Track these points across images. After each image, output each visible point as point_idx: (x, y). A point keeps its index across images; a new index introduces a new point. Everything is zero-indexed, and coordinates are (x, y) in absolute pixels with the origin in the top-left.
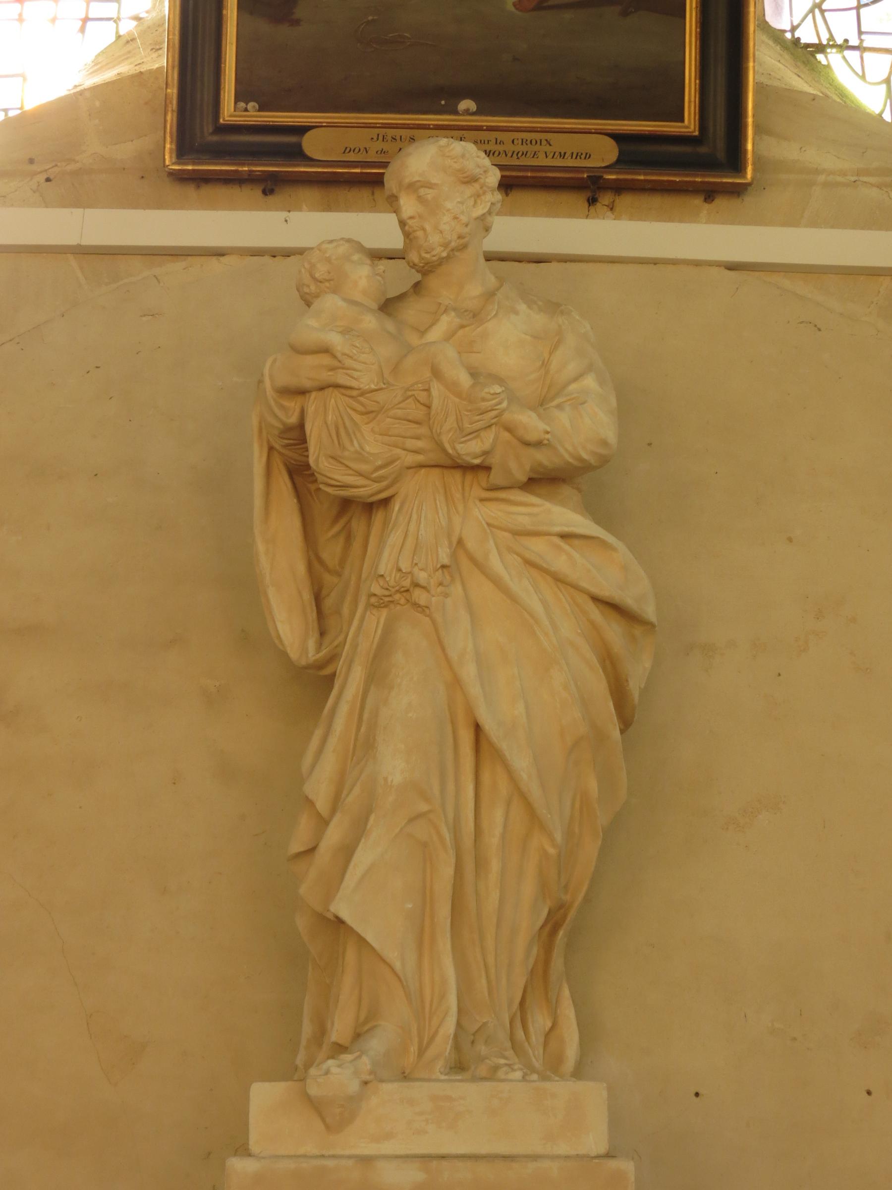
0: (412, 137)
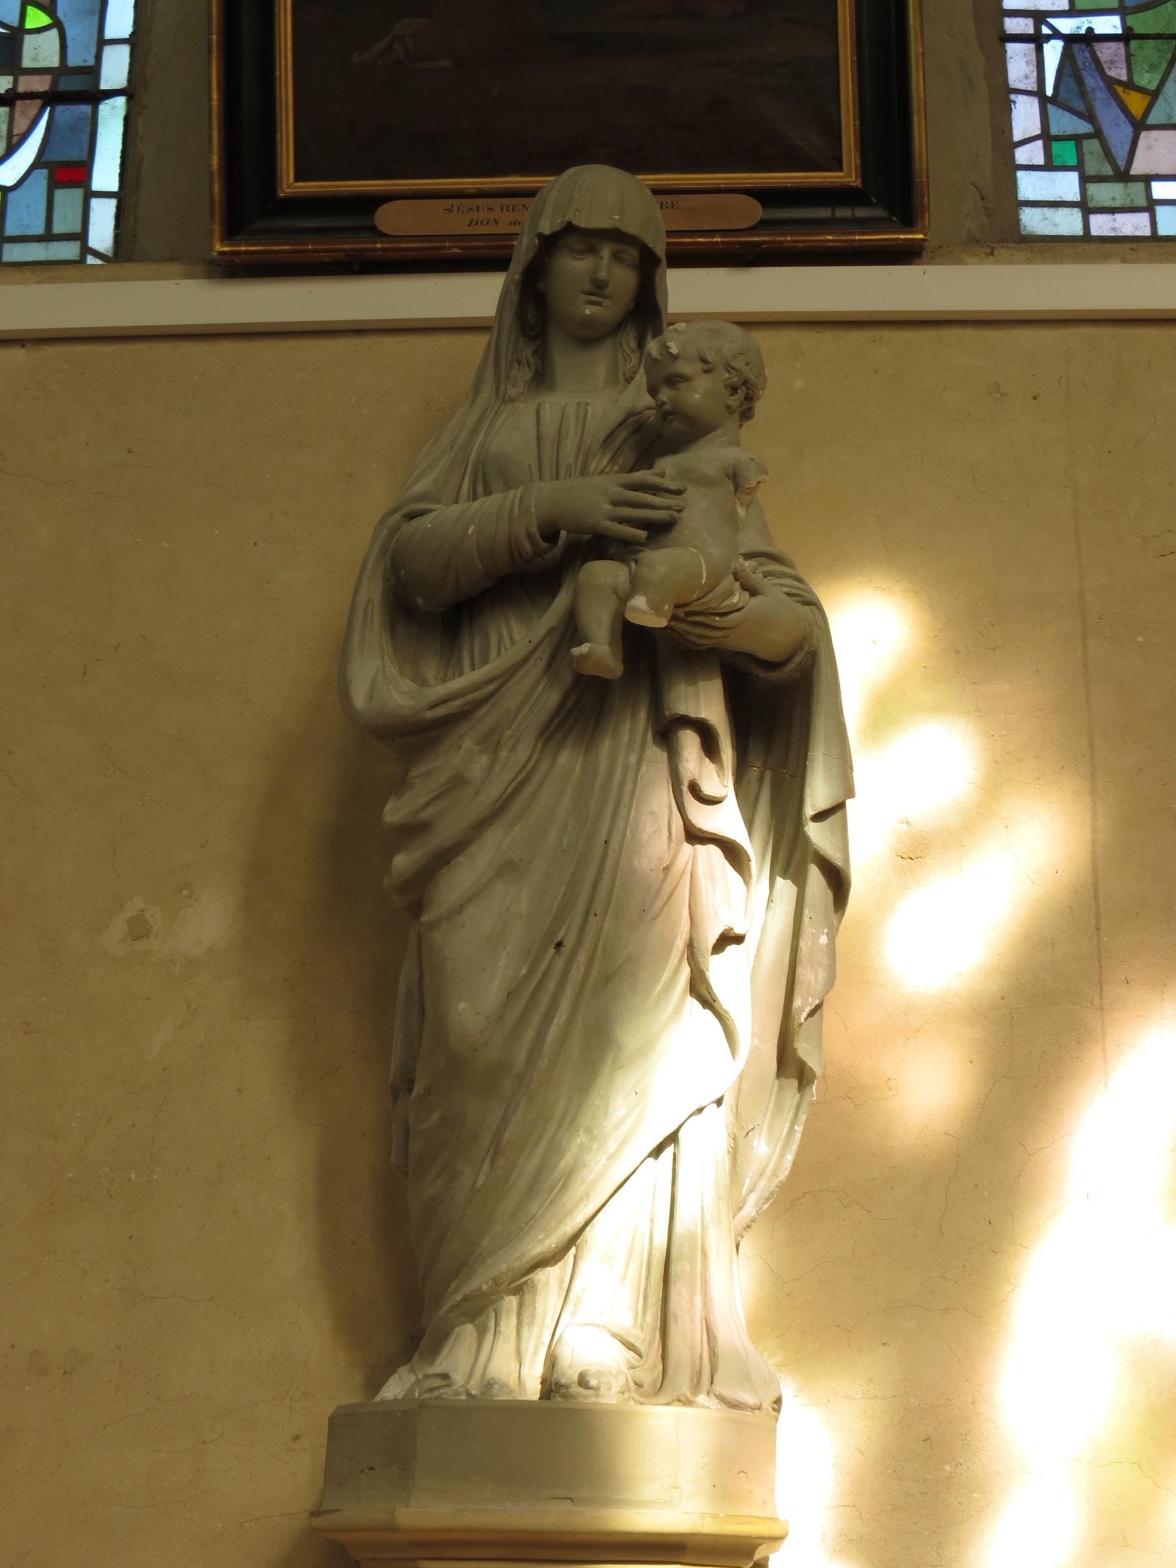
0: (471, 207)
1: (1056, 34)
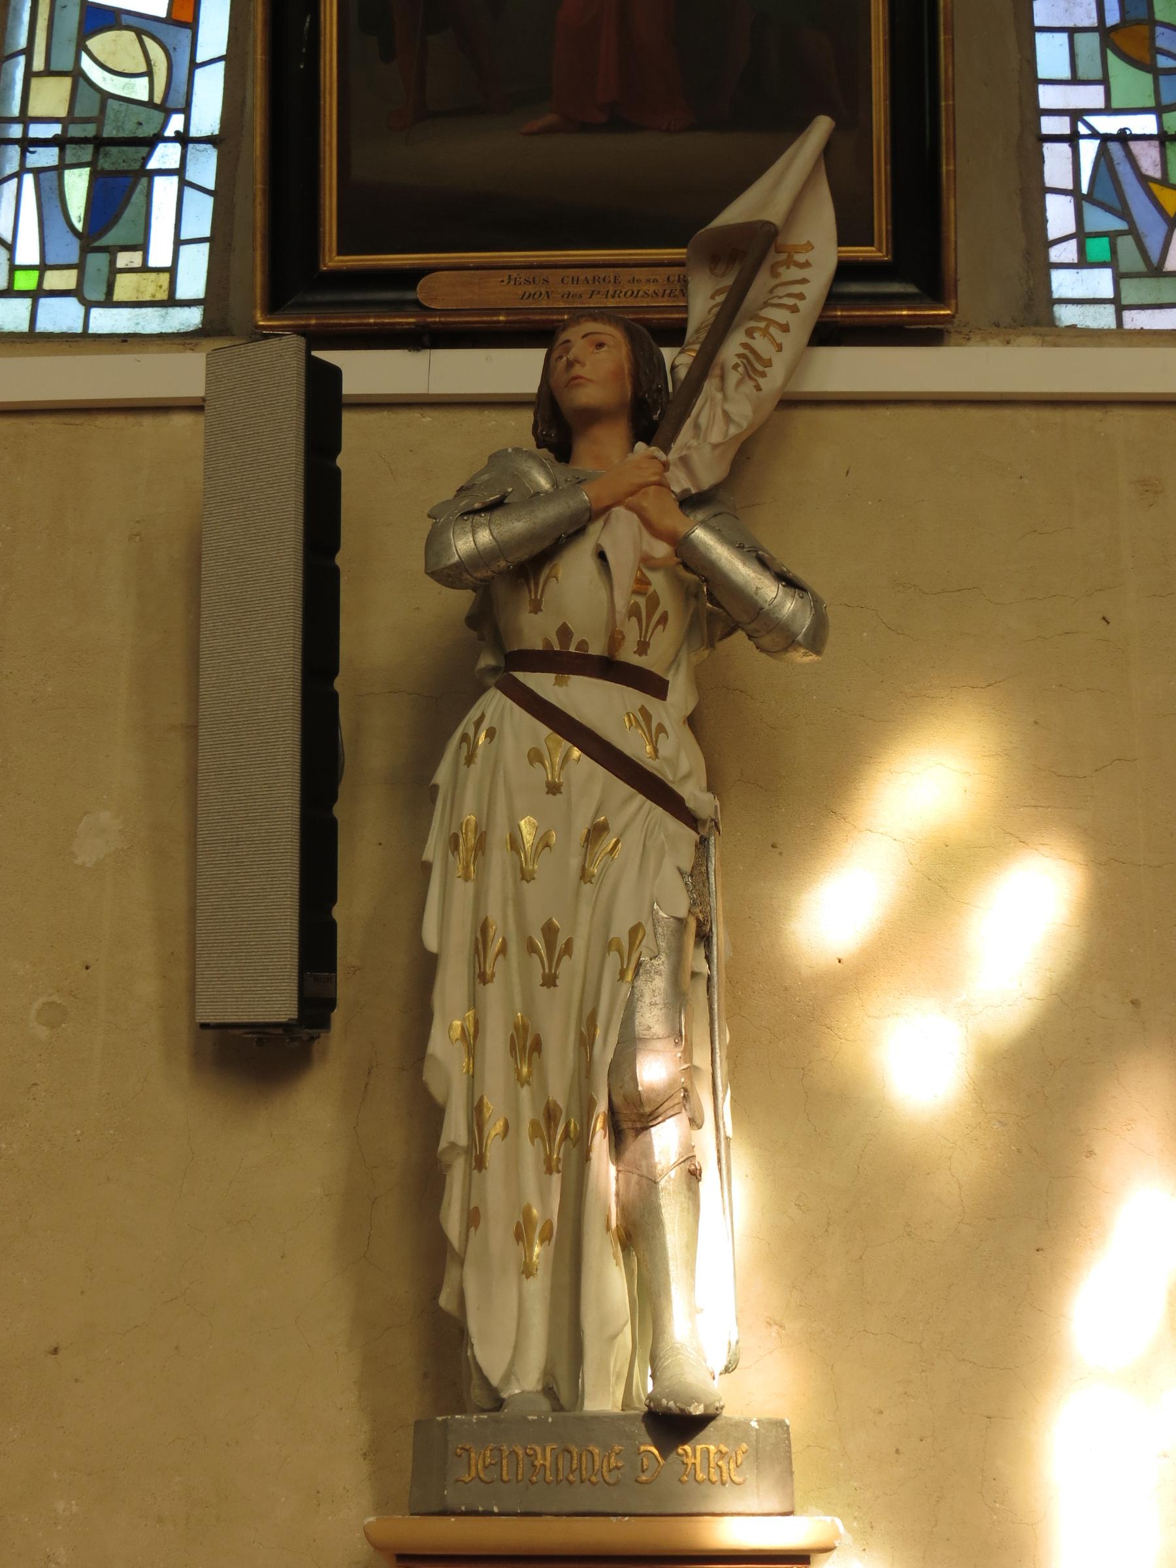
1: (1095, 134)
